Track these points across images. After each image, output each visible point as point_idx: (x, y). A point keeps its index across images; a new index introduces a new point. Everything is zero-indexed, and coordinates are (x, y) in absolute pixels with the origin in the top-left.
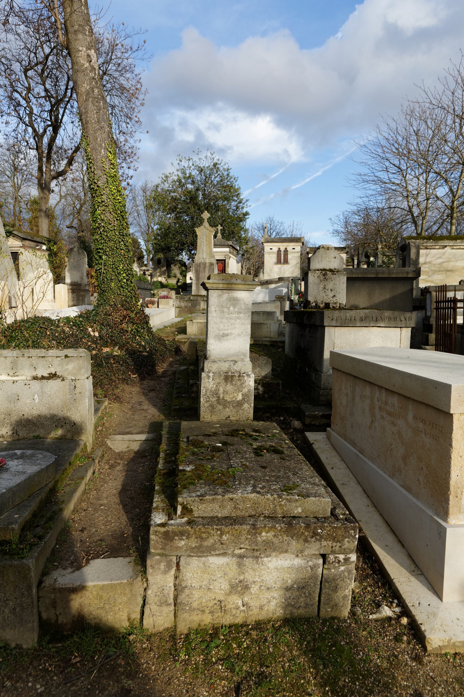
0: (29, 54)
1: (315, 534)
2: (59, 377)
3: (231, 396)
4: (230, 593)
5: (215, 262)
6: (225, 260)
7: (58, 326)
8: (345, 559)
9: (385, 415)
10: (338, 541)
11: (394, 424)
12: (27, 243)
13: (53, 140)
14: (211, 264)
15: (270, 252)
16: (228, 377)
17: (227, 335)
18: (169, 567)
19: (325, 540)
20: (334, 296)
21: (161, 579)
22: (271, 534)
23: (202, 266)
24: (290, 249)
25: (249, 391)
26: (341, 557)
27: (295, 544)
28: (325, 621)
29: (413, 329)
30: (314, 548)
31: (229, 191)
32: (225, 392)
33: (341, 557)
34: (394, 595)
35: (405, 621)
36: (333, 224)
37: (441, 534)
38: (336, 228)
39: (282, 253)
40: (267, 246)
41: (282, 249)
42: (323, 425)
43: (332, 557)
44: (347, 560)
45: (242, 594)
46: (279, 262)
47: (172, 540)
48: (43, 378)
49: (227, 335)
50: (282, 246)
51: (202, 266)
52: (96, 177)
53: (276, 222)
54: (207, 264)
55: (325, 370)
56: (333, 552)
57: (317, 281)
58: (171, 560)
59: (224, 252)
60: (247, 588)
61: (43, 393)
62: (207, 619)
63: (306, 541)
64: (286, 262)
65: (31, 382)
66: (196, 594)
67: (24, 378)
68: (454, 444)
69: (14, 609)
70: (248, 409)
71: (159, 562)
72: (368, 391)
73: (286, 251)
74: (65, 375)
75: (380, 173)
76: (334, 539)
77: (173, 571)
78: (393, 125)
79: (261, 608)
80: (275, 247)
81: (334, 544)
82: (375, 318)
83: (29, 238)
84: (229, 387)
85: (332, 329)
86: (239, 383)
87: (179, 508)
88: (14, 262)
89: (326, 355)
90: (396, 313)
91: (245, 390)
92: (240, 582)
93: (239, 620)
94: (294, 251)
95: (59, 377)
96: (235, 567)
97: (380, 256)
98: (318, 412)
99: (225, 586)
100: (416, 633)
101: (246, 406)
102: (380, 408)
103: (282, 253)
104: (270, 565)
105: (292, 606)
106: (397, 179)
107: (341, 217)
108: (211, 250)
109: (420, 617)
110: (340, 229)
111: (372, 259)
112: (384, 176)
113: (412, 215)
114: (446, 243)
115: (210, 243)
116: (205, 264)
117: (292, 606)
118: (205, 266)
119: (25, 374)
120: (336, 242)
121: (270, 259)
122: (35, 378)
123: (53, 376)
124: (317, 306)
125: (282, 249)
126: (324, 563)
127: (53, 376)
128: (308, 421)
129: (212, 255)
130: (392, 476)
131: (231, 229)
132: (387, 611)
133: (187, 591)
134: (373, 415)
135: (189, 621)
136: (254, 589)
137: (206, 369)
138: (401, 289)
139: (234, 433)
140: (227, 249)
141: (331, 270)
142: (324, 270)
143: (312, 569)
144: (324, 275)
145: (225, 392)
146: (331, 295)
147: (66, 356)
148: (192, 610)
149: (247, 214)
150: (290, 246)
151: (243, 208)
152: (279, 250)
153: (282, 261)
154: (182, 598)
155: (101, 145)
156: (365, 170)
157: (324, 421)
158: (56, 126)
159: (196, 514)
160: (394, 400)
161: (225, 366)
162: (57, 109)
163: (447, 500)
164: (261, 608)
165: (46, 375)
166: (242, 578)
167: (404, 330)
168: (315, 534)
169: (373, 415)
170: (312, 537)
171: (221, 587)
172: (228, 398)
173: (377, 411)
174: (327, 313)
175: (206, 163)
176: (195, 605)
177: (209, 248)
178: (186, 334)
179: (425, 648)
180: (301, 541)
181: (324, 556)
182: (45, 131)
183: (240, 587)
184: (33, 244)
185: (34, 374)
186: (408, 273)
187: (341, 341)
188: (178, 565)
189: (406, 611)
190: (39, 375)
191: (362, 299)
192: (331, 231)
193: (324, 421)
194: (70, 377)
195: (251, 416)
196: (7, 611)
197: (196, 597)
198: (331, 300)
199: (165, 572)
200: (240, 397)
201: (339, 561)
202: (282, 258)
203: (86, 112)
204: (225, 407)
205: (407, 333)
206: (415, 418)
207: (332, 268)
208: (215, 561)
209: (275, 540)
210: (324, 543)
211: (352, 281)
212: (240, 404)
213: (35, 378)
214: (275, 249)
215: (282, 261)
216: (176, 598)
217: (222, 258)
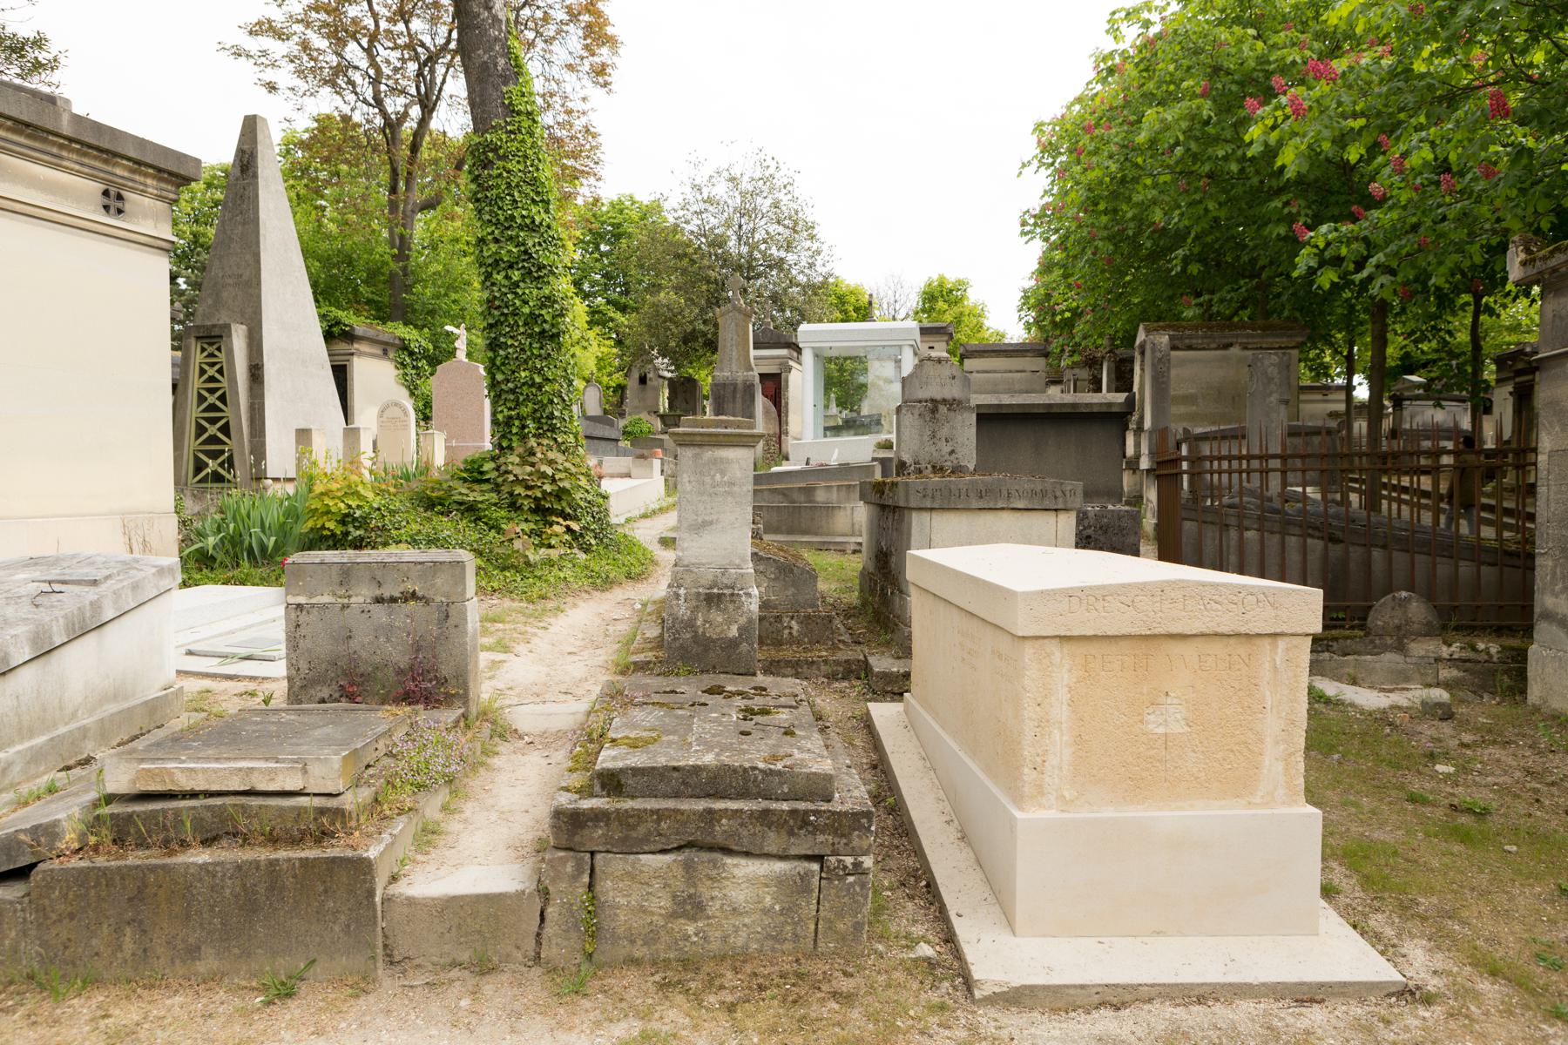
3: (718, 630)
4: (673, 915)
6: (779, 375)
8: (854, 865)
10: (843, 835)
13: (423, 122)
14: (749, 388)
17: (711, 523)
18: (579, 871)
19: (823, 832)
20: (953, 452)
25: (750, 621)
26: (849, 860)
33: (849, 860)
42: (895, 687)
43: (833, 859)
45: (694, 919)
48: (393, 600)
49: (711, 523)
54: (740, 387)
56: (835, 853)
58: (582, 859)
59: (778, 357)
63: (791, 833)
65: (372, 607)
69: (348, 926)
77: (586, 879)
79: (725, 939)
81: (836, 840)
82: (1005, 493)
85: (926, 516)
86: (731, 607)
88: (254, 141)
92: (690, 896)
95: (421, 599)
96: (679, 872)
104: (736, 871)
105: (773, 938)
117: (773, 938)
122: (379, 600)
126: (822, 869)
142: (933, 400)
143: (802, 878)
148: (615, 938)
158: (428, 105)
162: (432, 71)
166: (692, 891)
167: (1063, 517)
170: (801, 828)
175: (747, 170)
176: (620, 931)
180: (784, 833)
183: (690, 907)
185: (378, 592)
196: (337, 928)
200: (734, 632)
201: (845, 867)
205: (1067, 523)
207: (948, 396)
210: (820, 838)
213: (379, 600)
217: (773, 369)
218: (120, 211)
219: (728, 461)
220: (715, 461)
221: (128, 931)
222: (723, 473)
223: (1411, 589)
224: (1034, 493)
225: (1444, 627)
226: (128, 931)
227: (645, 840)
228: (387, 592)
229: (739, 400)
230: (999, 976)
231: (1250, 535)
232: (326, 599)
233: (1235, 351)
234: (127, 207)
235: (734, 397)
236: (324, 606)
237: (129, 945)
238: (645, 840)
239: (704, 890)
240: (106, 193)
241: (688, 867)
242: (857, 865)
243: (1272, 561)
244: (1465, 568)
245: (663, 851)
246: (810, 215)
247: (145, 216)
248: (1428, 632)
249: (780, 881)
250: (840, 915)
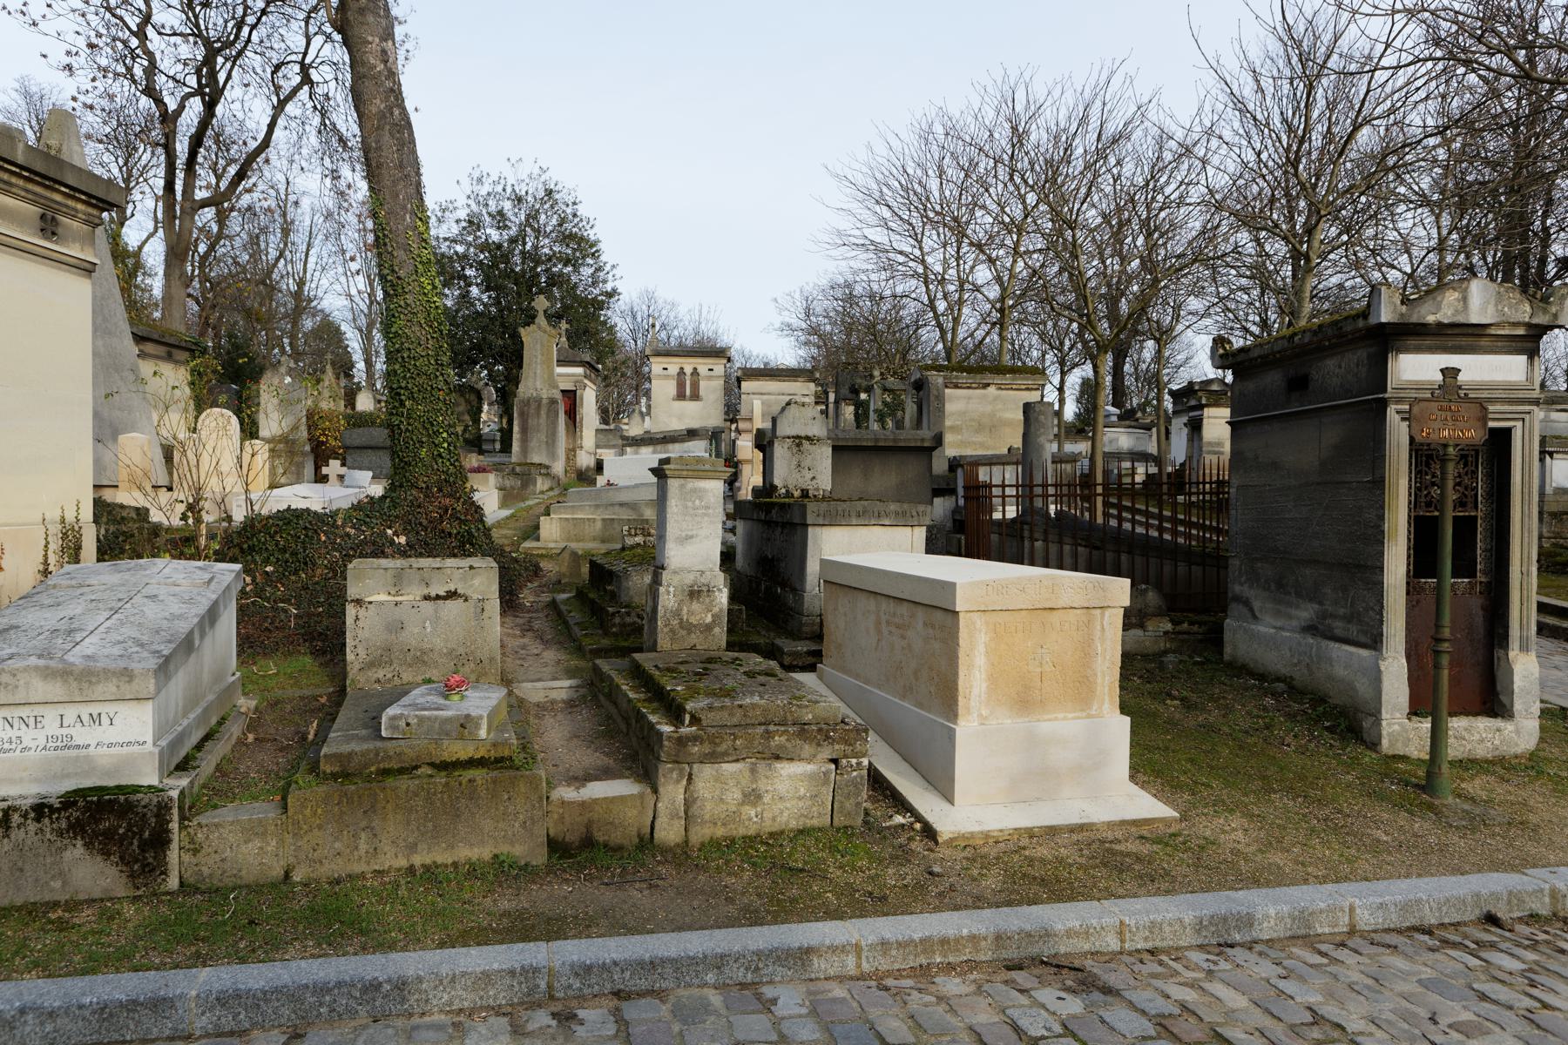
0: (293, 57)
1: (828, 737)
2: (460, 596)
4: (743, 803)
5: (559, 396)
7: (334, 525)
9: (893, 629)
11: (903, 637)
12: (149, 348)
14: (553, 402)
15: (662, 376)
16: (694, 593)
21: (672, 792)
22: (783, 739)
23: (533, 406)
24: (703, 370)
27: (807, 749)
28: (838, 830)
29: (930, 530)
30: (827, 752)
31: (580, 246)
32: (690, 613)
33: (854, 761)
34: (902, 804)
35: (918, 826)
36: (781, 310)
37: (951, 735)
38: (787, 320)
39: (688, 378)
40: (656, 366)
41: (688, 370)
44: (859, 764)
45: (754, 805)
46: (681, 396)
47: (685, 746)
48: (438, 597)
50: (688, 365)
51: (533, 406)
52: (396, 262)
53: (660, 301)
55: (808, 587)
56: (846, 756)
57: (788, 454)
60: (759, 797)
61: (438, 618)
62: (720, 832)
63: (819, 745)
64: (695, 396)
66: (708, 806)
67: (411, 597)
68: (961, 642)
70: (720, 635)
71: (671, 770)
72: (871, 604)
73: (695, 372)
74: (469, 593)
75: (872, 230)
76: (846, 742)
77: (684, 782)
78: (895, 143)
79: (774, 819)
80: (674, 365)
83: (156, 337)
84: (695, 606)
85: (818, 529)
87: (687, 717)
89: (813, 568)
90: (906, 506)
91: (716, 610)
93: (752, 832)
94: (712, 375)
95: (460, 596)
96: (747, 774)
97: (878, 390)
98: (802, 647)
99: (738, 795)
100: (929, 832)
101: (717, 630)
102: (888, 623)
103: (688, 378)
106: (906, 245)
107: (797, 295)
108: (552, 372)
109: (930, 818)
110: (796, 323)
111: (863, 396)
112: (880, 236)
113: (935, 312)
114: (988, 378)
115: (550, 359)
116: (539, 401)
118: (539, 406)
119: (413, 594)
120: (788, 354)
121: (662, 389)
122: (427, 598)
123: (452, 595)
124: (789, 494)
125: (688, 370)
127: (452, 595)
128: (787, 660)
129: (551, 381)
130: (903, 697)
131: (585, 325)
132: (899, 819)
133: (699, 803)
134: (879, 632)
135: (700, 834)
136: (767, 799)
137: (664, 582)
138: (913, 467)
139: (710, 660)
140: (580, 370)
141: (808, 438)
142: (798, 437)
144: (798, 445)
145: (690, 613)
146: (809, 475)
147: (471, 567)
148: (704, 823)
149: (612, 294)
150: (703, 365)
151: (605, 282)
152: (682, 372)
153: (688, 392)
154: (694, 810)
155: (404, 207)
156: (846, 224)
157: (811, 660)
159: (704, 723)
160: (904, 609)
161: (689, 579)
163: (956, 702)
164: (774, 819)
165: (442, 593)
167: (917, 529)
168: (828, 737)
169: (879, 632)
171: (734, 795)
172: (693, 620)
173: (884, 625)
174: (811, 507)
176: (707, 817)
177: (547, 368)
178: (538, 539)
179: (937, 843)
181: (835, 761)
182: (181, 107)
183: (752, 797)
184: (161, 350)
185: (426, 592)
186: (923, 440)
187: (836, 546)
188: (690, 775)
189: (918, 817)
190: (433, 594)
191: (855, 481)
192: (777, 325)
193: (811, 660)
194: (475, 596)
195: (724, 644)
197: (708, 807)
198: (810, 486)
199: (678, 781)
200: (709, 619)
202: (687, 390)
203: (379, 148)
204: (690, 632)
205: (920, 534)
206: (925, 624)
208: (729, 768)
209: (788, 745)
211: (840, 450)
212: (709, 628)
213: (427, 598)
214: (673, 369)
215: (688, 392)
216: (686, 813)
217: (570, 387)
218: (54, 234)
219: (705, 490)
220: (694, 490)
221: (363, 835)
222: (701, 499)
223: (1147, 583)
224: (897, 513)
225: (1170, 609)
226: (363, 835)
227: (726, 754)
228: (436, 590)
229: (543, 413)
230: (953, 829)
231: (1038, 544)
232: (383, 597)
233: (992, 390)
234: (60, 230)
235: (538, 414)
236: (382, 603)
237: (363, 847)
238: (726, 754)
239: (762, 785)
240: (43, 217)
241: (753, 771)
242: (859, 764)
243: (1068, 560)
244: (1182, 568)
245: (737, 761)
246: (591, 234)
247: (74, 241)
248: (1159, 614)
249: (811, 777)
250: (848, 797)
